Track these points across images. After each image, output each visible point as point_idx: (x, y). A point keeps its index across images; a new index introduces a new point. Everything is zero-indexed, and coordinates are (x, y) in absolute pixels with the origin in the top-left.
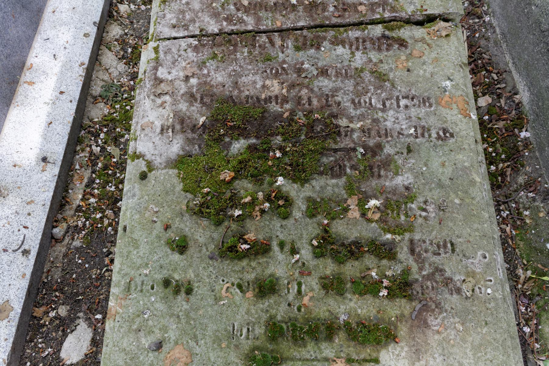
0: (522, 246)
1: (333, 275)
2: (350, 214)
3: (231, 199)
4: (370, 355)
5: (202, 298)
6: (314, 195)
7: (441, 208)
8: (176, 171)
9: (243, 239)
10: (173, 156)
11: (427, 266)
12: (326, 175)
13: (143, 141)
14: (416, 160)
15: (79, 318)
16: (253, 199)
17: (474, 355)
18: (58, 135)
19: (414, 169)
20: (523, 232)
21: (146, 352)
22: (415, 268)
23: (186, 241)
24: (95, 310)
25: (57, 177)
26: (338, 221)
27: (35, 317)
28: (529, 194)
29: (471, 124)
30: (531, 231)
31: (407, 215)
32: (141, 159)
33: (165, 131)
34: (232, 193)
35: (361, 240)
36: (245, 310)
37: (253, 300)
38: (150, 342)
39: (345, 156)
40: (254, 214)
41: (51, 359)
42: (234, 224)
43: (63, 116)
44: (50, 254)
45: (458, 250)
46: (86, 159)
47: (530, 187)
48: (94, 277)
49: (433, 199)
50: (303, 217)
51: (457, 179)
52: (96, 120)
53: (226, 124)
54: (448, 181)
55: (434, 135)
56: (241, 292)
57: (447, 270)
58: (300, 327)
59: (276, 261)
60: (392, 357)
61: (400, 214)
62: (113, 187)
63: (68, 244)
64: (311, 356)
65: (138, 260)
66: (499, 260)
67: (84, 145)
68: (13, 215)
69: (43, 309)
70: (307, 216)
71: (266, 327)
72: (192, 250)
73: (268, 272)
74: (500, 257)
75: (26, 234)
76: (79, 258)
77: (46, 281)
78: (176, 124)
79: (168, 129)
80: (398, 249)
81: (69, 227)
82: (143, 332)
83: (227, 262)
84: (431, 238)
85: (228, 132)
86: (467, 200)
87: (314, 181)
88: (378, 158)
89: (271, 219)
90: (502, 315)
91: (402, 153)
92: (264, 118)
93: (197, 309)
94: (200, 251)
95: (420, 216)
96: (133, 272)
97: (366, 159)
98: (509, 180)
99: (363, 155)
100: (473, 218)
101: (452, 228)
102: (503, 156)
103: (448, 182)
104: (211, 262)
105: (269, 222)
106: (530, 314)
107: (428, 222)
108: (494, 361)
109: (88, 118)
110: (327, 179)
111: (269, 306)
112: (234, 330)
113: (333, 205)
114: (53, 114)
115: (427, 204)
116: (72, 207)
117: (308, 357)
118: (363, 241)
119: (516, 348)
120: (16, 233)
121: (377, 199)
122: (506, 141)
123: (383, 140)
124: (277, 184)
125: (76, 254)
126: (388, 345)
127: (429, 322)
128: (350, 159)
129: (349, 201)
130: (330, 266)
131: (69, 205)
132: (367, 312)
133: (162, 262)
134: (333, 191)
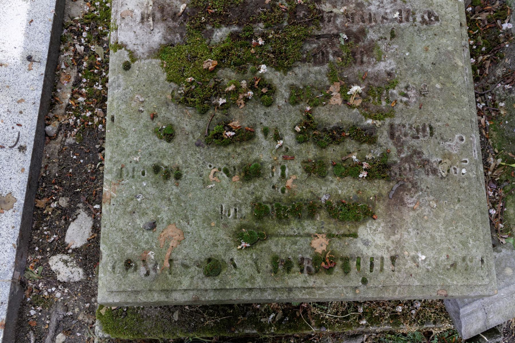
0: (494, 136)
1: (315, 159)
2: (332, 101)
3: (215, 88)
4: (349, 231)
5: (191, 182)
6: (297, 83)
7: (422, 93)
8: (159, 61)
9: (229, 127)
10: (155, 46)
11: (406, 149)
12: (309, 62)
13: (124, 31)
14: (400, 45)
15: (79, 208)
16: (236, 88)
17: (445, 229)
18: (40, 34)
19: (397, 54)
20: (497, 123)
21: (141, 232)
22: (394, 151)
23: (173, 130)
24: (93, 201)
25: (43, 76)
26: (320, 108)
27: (39, 208)
28: (506, 86)
29: (457, 6)
30: (505, 122)
31: (388, 101)
32: (123, 49)
33: (145, 20)
34: (215, 81)
35: (343, 125)
36: (232, 192)
37: (240, 183)
38: (144, 222)
39: (328, 43)
40: (238, 102)
41: (57, 244)
42: (218, 112)
43: (43, 14)
44: (46, 151)
45: (436, 134)
46: (71, 58)
47: (508, 79)
48: (89, 171)
49: (415, 84)
50: (287, 105)
51: (439, 64)
52: (77, 18)
53: (208, 11)
54: (430, 65)
55: (419, 19)
56: (227, 176)
57: (424, 153)
58: (284, 207)
59: (261, 146)
60: (369, 232)
61: (381, 99)
62: (100, 86)
63: (62, 141)
64: (295, 232)
65: (128, 148)
66: (475, 142)
67: (67, 45)
68: (6, 114)
69: (45, 200)
70: (291, 103)
71: (252, 207)
72: (179, 138)
73: (253, 157)
74: (476, 139)
75: (21, 131)
76: (73, 154)
77: (44, 175)
78: (156, 12)
79: (148, 18)
80: (378, 134)
81: (61, 125)
82: (138, 213)
83: (214, 149)
84: (411, 122)
85: (209, 19)
86: (448, 85)
87: (297, 68)
88: (361, 44)
89: (254, 107)
90: (474, 192)
91: (386, 39)
92: (246, 5)
93: (187, 193)
94: (187, 139)
95: (401, 101)
96: (124, 160)
97: (349, 46)
98: (487, 73)
99: (346, 41)
100: (453, 102)
101: (431, 112)
102: (484, 49)
103: (430, 67)
104: (197, 149)
105: (253, 110)
106: (497, 198)
107: (408, 107)
108: (464, 234)
109: (69, 16)
110: (309, 66)
111: (254, 188)
112: (222, 211)
113: (315, 92)
114: (33, 11)
115: (409, 89)
116: (62, 106)
117: (292, 233)
118: (345, 126)
119: (485, 222)
120: (11, 130)
121: (359, 85)
122: (488, 33)
123: (367, 25)
124: (260, 72)
125: (70, 151)
126: (366, 222)
127: (405, 200)
128: (333, 45)
129: (332, 88)
130: (313, 151)
131: (59, 104)
132: (347, 193)
133: (151, 150)
134: (315, 78)
